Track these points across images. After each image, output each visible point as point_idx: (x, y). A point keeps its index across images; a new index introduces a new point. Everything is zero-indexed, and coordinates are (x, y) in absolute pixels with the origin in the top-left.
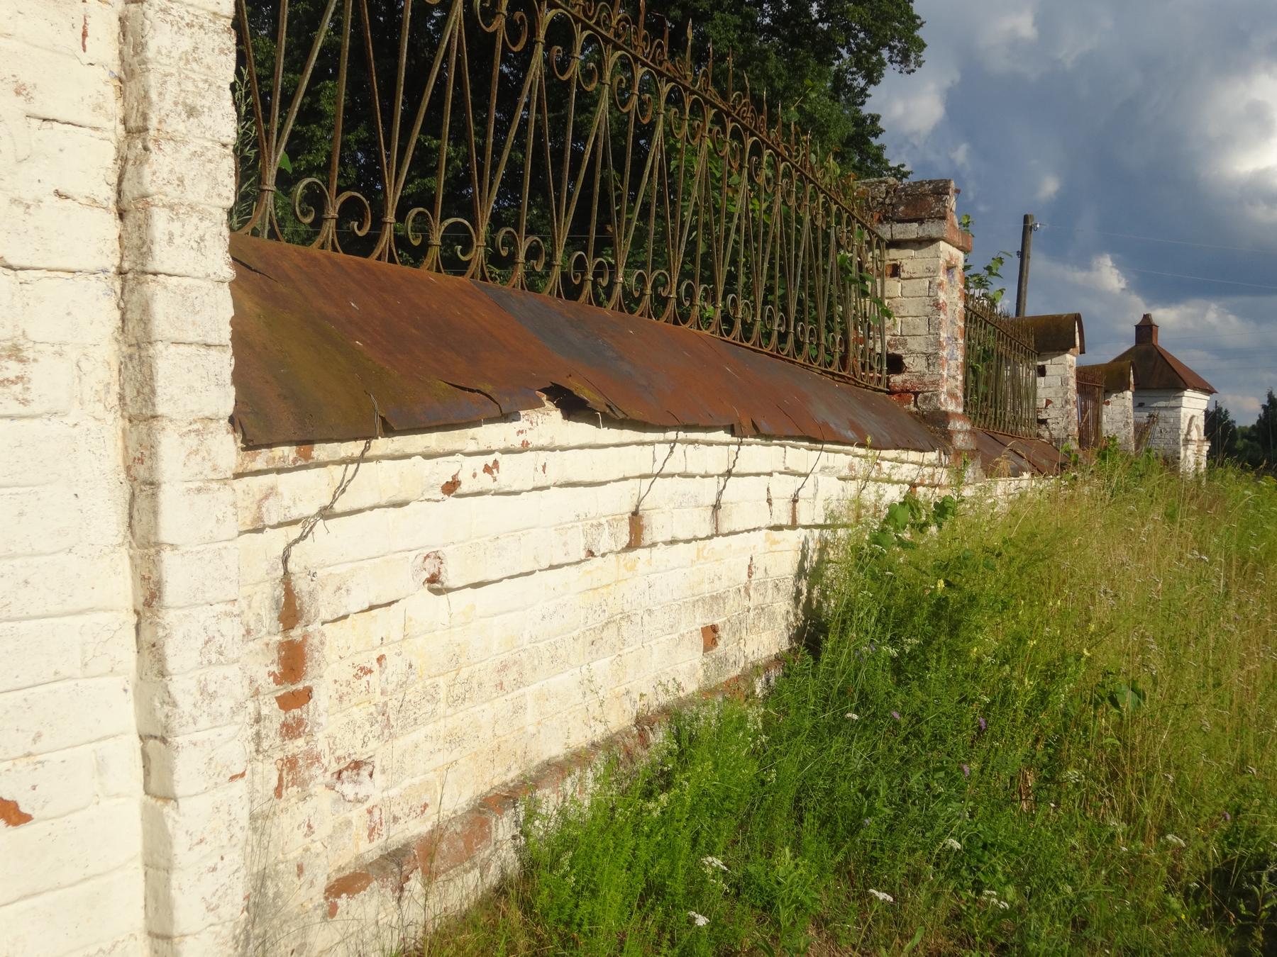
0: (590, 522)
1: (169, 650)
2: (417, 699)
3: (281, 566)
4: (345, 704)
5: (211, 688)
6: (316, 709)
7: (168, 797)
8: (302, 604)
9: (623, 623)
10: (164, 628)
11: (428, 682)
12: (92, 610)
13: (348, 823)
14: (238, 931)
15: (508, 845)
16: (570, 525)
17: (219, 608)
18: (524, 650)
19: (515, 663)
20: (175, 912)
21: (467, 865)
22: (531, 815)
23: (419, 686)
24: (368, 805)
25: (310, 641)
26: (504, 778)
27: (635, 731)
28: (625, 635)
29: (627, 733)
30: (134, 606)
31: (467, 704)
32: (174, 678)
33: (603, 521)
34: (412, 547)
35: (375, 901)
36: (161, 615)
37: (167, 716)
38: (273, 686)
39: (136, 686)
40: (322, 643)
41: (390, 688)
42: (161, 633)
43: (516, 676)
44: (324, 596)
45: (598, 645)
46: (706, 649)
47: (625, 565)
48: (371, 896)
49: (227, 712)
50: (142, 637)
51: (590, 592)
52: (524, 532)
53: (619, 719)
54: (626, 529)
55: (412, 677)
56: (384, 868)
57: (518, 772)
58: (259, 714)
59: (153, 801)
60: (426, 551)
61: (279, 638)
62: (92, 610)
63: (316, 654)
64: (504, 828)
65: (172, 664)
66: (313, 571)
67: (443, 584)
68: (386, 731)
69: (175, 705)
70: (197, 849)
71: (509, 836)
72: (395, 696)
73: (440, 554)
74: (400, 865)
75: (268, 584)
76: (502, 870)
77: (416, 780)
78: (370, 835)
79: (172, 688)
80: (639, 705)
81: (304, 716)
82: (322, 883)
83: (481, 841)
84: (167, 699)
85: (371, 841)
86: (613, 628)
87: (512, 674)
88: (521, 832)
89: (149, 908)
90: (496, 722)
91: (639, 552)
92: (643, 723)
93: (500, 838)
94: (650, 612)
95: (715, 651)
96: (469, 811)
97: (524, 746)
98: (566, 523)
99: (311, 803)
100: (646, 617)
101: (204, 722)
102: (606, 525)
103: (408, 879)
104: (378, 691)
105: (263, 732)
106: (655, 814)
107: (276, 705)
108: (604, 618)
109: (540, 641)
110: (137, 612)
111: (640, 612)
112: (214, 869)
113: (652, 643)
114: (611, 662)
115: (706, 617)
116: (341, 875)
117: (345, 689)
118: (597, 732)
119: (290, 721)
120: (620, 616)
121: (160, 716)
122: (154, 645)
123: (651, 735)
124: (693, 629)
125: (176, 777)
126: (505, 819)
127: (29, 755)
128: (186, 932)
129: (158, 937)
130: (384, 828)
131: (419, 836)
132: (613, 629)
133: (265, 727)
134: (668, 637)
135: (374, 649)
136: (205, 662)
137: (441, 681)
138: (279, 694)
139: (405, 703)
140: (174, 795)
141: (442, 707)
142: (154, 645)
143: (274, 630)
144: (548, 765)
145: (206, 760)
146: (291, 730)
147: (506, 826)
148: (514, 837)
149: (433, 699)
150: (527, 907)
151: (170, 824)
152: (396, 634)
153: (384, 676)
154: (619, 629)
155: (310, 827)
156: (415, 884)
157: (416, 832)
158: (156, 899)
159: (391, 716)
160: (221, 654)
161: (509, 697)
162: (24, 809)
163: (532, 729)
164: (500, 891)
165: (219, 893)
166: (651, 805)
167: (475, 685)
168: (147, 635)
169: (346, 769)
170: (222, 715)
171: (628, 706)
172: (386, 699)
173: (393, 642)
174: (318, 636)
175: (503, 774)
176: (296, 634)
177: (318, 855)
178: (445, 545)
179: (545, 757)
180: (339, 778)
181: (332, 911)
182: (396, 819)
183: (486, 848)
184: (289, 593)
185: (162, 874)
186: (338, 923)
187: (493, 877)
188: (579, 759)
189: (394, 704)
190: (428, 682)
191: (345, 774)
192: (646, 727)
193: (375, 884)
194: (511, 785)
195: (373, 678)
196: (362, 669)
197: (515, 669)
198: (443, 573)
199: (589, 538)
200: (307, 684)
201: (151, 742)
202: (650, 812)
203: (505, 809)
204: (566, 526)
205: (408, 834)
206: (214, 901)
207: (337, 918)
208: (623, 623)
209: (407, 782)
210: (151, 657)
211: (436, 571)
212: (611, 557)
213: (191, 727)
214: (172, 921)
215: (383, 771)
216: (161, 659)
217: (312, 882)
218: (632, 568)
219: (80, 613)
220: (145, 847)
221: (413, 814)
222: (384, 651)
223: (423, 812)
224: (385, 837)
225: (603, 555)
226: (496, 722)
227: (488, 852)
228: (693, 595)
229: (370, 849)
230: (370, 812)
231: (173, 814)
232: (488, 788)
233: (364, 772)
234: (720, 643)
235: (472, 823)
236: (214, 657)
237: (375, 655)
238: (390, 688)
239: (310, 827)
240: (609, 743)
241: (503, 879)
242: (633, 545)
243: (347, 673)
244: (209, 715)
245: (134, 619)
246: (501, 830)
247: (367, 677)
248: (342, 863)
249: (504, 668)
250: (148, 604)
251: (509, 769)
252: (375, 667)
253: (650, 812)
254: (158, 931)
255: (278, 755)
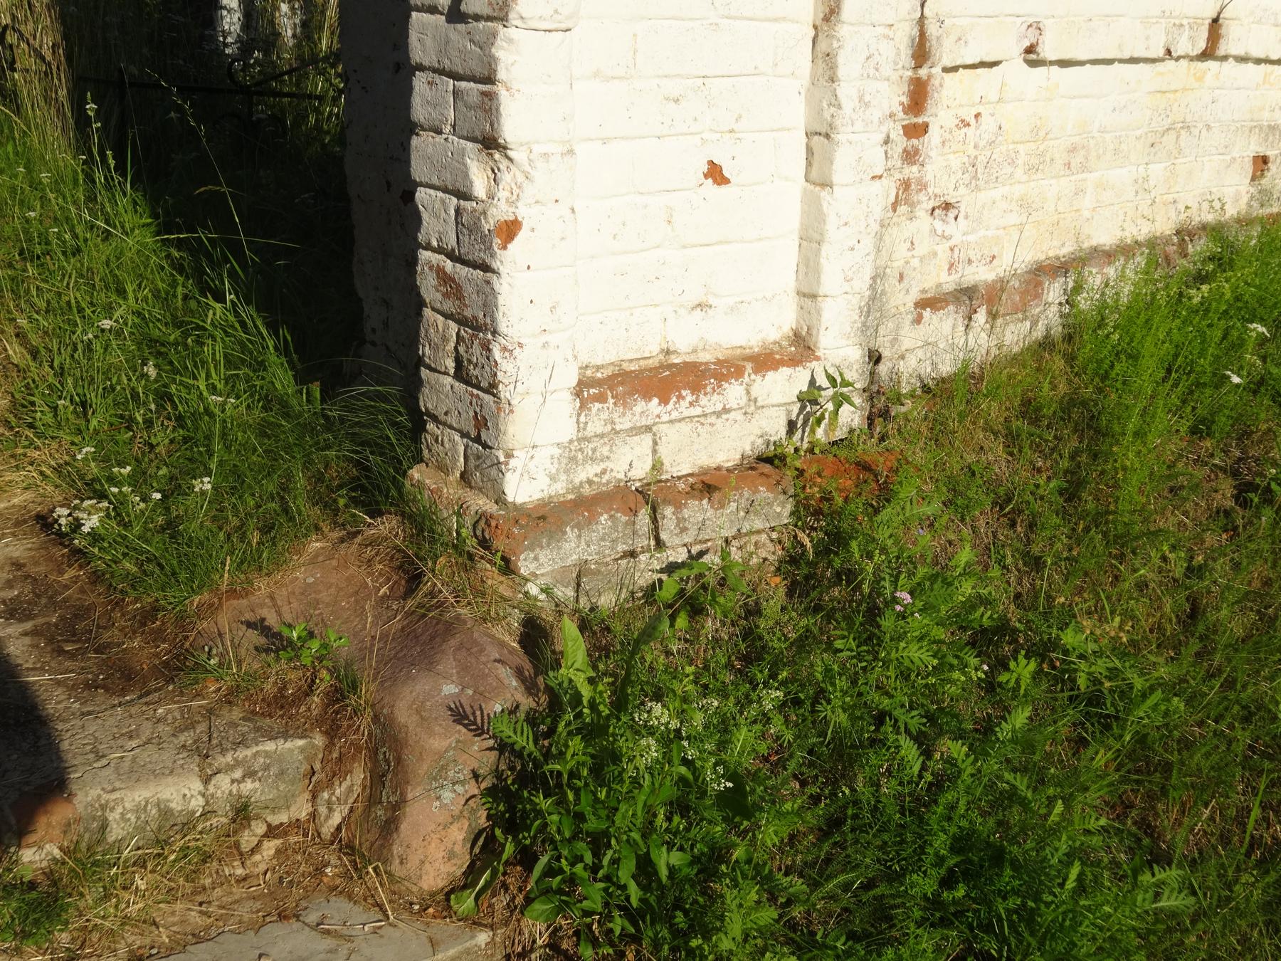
0: (1173, 21)
1: (841, 60)
2: (1001, 160)
3: (919, 8)
4: (946, 149)
5: (867, 98)
6: (929, 142)
7: (826, 184)
8: (930, 47)
9: (1183, 132)
10: (839, 40)
11: (1011, 147)
12: (784, 19)
13: (935, 254)
14: (863, 304)
15: (1054, 308)
16: (1154, 21)
17: (880, 30)
18: (1093, 138)
19: (1084, 147)
20: (822, 276)
21: (1020, 316)
22: (1078, 289)
23: (1004, 148)
24: (951, 243)
25: (933, 81)
26: (1058, 252)
27: (1175, 239)
28: (1183, 145)
29: (1167, 241)
30: (814, 21)
31: (1039, 175)
32: (842, 84)
33: (1185, 22)
34: (1021, 13)
35: (950, 322)
36: (836, 29)
37: (832, 116)
38: (901, 115)
39: (809, 90)
40: (941, 86)
41: (982, 143)
42: (835, 45)
43: (1082, 160)
44: (948, 43)
45: (1157, 148)
46: (1253, 179)
47: (1195, 74)
48: (948, 317)
49: (876, 120)
50: (818, 48)
51: (1159, 95)
52: (1115, 18)
53: (1164, 225)
54: (1204, 34)
55: (1000, 138)
56: (957, 299)
57: (1071, 249)
58: (888, 137)
59: (812, 187)
60: (1031, 20)
61: (910, 73)
62: (784, 19)
63: (936, 95)
64: (1054, 292)
65: (841, 72)
66: (942, 19)
67: (1038, 55)
68: (973, 182)
69: (840, 107)
70: (843, 228)
71: (1057, 302)
72: (984, 153)
73: (1041, 25)
74: (971, 299)
75: (907, 23)
76: (1048, 329)
77: (989, 233)
78: (949, 269)
79: (838, 93)
80: (1183, 217)
81: (920, 147)
82: (914, 295)
83: (1033, 300)
84: (833, 101)
85: (950, 274)
86: (1173, 135)
87: (1077, 160)
88: (1067, 302)
89: (800, 272)
90: (1059, 199)
91: (1211, 65)
92: (1185, 234)
93: (1050, 300)
94: (1208, 127)
95: (1264, 181)
96: (1026, 272)
97: (1078, 227)
98: (1152, 17)
99: (916, 223)
100: (1204, 132)
101: (859, 126)
102: (1187, 27)
103: (975, 312)
104: (972, 144)
105: (890, 153)
106: (1196, 300)
107: (901, 132)
108: (1167, 123)
109: (1107, 132)
110: (815, 27)
111: (1200, 125)
112: (852, 249)
113: (1207, 158)
114: (1166, 168)
115: (1260, 145)
116: (924, 296)
117: (947, 136)
118: (1142, 232)
119: (909, 148)
120: (1181, 125)
121: (827, 115)
122: (828, 55)
123: (1190, 246)
124: (1245, 154)
125: (834, 167)
126: (1056, 285)
127: (732, 131)
128: (828, 294)
129: (804, 295)
130: (960, 266)
131: (986, 282)
132: (1172, 136)
133: (891, 149)
134: (1221, 157)
135: (973, 105)
136: (865, 75)
137: (1020, 147)
138: (905, 123)
139: (991, 161)
140: (832, 182)
141: (1019, 173)
142: (828, 55)
143: (908, 66)
144: (1095, 250)
145: (857, 158)
146: (910, 156)
147: (1057, 291)
148: (1060, 304)
149: (1013, 163)
150: (1070, 359)
151: (825, 205)
152: (993, 97)
153: (978, 132)
154: (1178, 138)
155: (912, 243)
156: (981, 317)
157: (983, 278)
158: (807, 266)
159: (979, 170)
160: (877, 70)
161: (1073, 178)
162: (726, 173)
163: (1086, 214)
164: (1046, 344)
165: (854, 269)
166: (1193, 292)
167: (1048, 160)
168: (823, 46)
169: (939, 207)
170: (872, 122)
171: (1173, 215)
172: (977, 153)
173: (989, 103)
174: (939, 78)
175: (1061, 248)
176: (923, 72)
177: (915, 269)
178: (1047, 18)
179: (1094, 243)
180: (932, 214)
181: (918, 320)
182: (970, 261)
183: (1037, 306)
184: (922, 34)
185: (815, 245)
186: (922, 328)
187: (1039, 333)
188: (1125, 250)
189: (982, 159)
190: (1011, 147)
191: (937, 212)
192: (1187, 238)
193: (951, 308)
194: (1063, 260)
195: (970, 131)
196: (963, 121)
197: (1083, 152)
198: (1040, 45)
199: (1170, 36)
200: (926, 119)
201: (816, 138)
202: (1190, 299)
203: (1057, 276)
204: (1151, 20)
205: (977, 278)
206: (850, 274)
207: (921, 326)
208: (1183, 132)
209: (982, 232)
210: (824, 65)
211: (1034, 41)
212: (1183, 62)
213: (850, 129)
214: (819, 283)
215: (966, 217)
216: (832, 67)
217: (908, 291)
218: (1200, 79)
219: (776, 20)
220: (802, 224)
221: (983, 262)
222: (980, 109)
223: (991, 262)
224: (960, 275)
225: (1178, 59)
226: (1059, 199)
227: (1038, 310)
228: (1252, 120)
229: (949, 282)
230: (952, 250)
231: (828, 197)
232: (1043, 257)
233: (952, 214)
234: (1268, 174)
235: (1028, 282)
236: (872, 72)
237: (974, 112)
238: (982, 143)
239: (912, 243)
240: (1152, 243)
241: (1046, 337)
242: (1207, 54)
243: (951, 122)
244: (863, 120)
245: (812, 33)
246: (1051, 293)
247: (964, 130)
248: (927, 285)
249: (1073, 150)
250: (827, 19)
251: (1063, 245)
252: (973, 121)
253: (1190, 299)
254: (806, 291)
255: (898, 176)
